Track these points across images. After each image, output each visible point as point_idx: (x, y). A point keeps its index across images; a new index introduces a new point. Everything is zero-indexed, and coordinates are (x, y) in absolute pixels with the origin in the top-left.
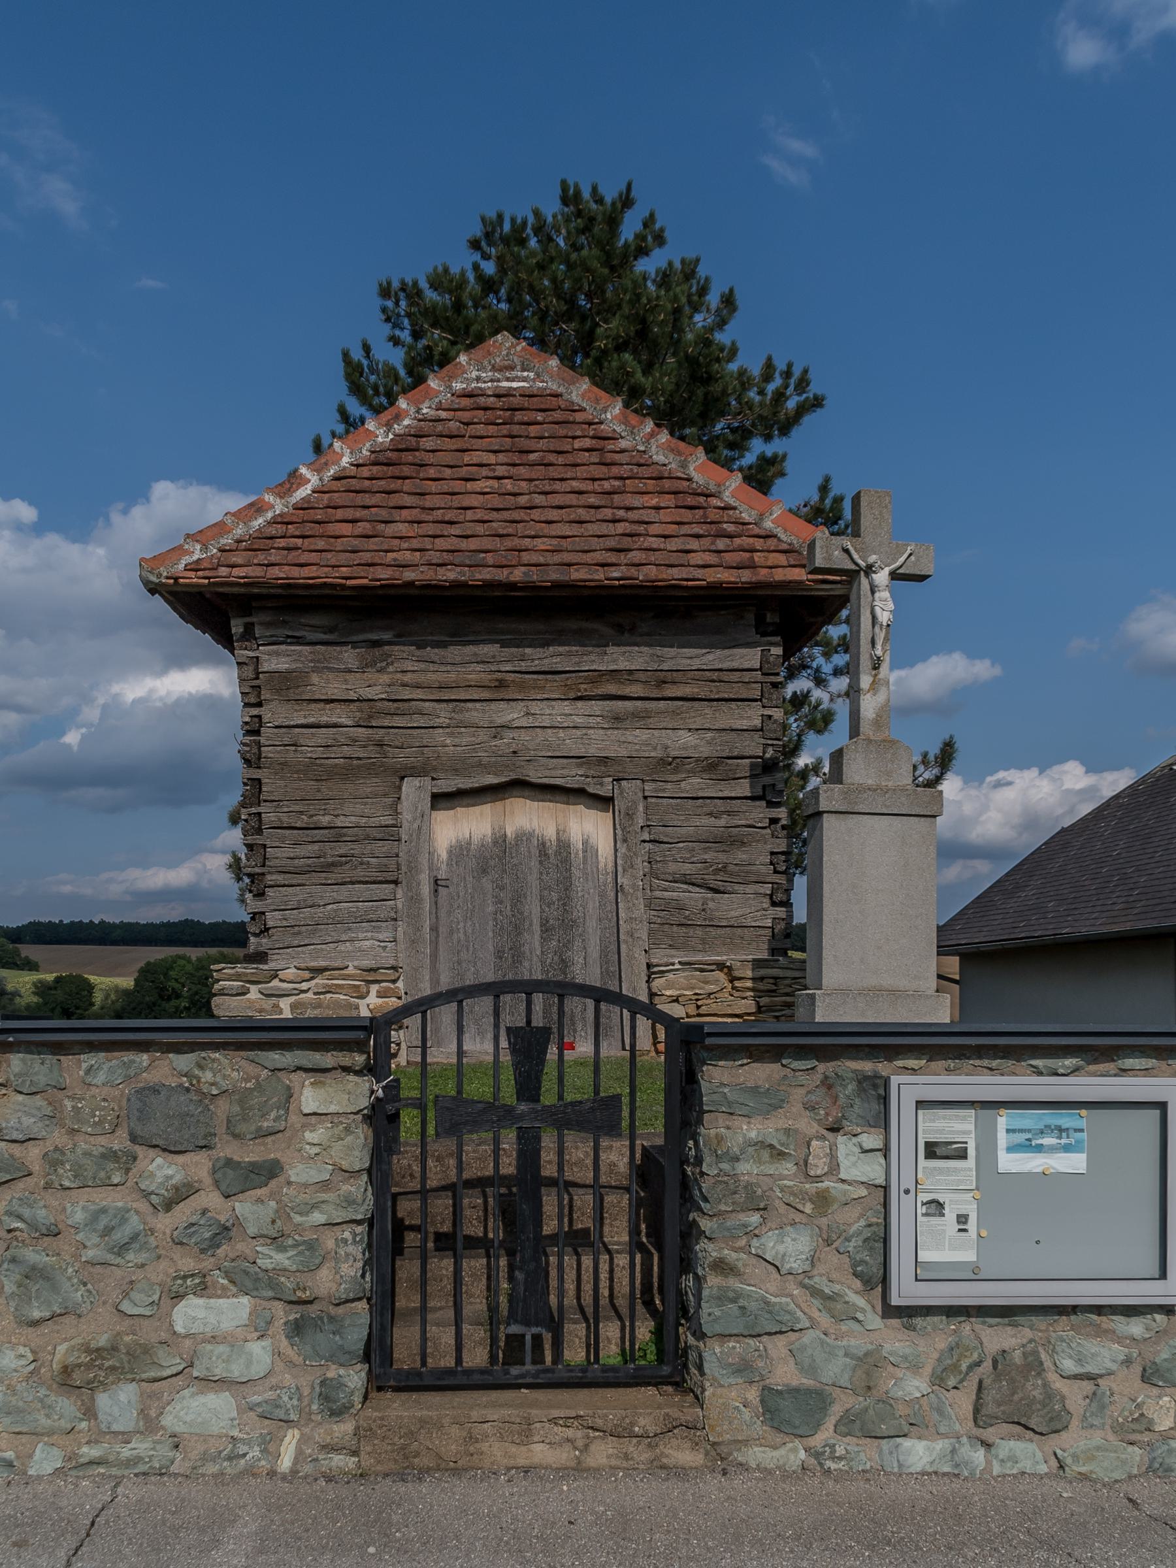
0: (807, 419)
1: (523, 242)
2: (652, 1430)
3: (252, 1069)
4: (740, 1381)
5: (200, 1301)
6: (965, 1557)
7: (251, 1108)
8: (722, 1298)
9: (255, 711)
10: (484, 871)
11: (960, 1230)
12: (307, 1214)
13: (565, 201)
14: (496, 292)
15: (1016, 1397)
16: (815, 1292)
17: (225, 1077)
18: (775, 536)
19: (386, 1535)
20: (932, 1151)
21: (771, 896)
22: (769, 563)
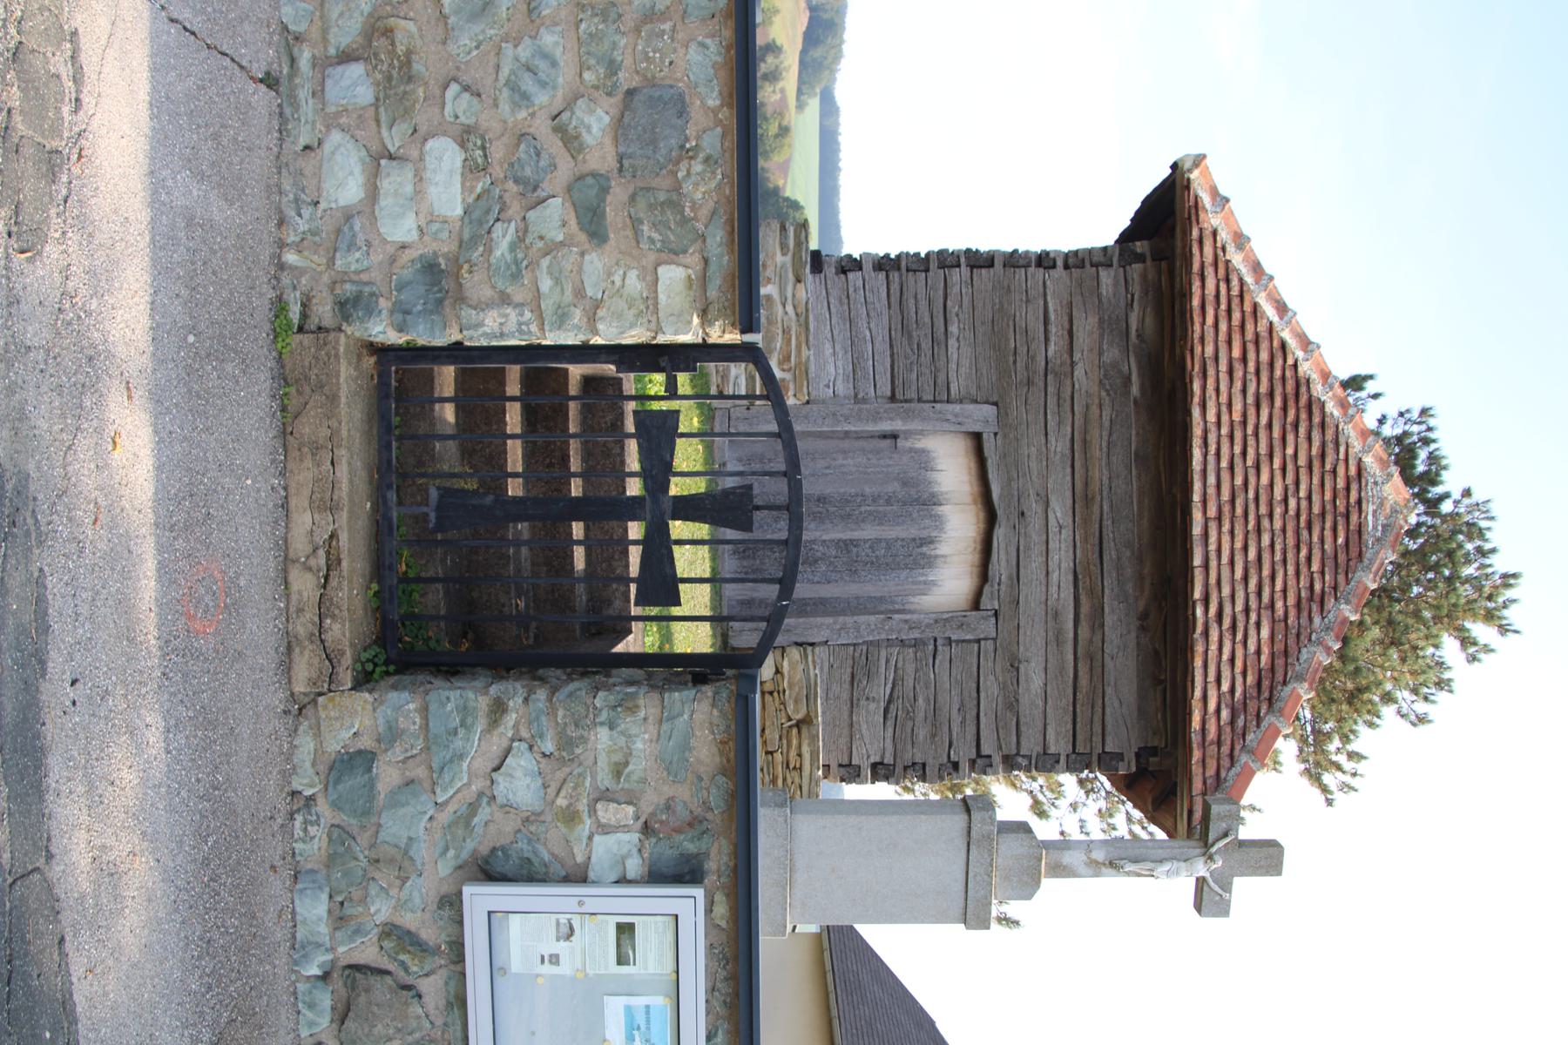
0: (1316, 791)
1: (1470, 538)
2: (328, 637)
3: (704, 213)
4: (381, 729)
5: (459, 163)
6: (200, 958)
7: (663, 212)
8: (464, 710)
9: (1060, 263)
10: (905, 484)
11: (543, 958)
12: (550, 273)
13: (1505, 576)
14: (1426, 513)
15: (375, 1009)
16: (473, 807)
17: (696, 185)
18: (1232, 765)
19: (209, 355)
20: (625, 931)
21: (881, 763)
22: (1208, 760)
